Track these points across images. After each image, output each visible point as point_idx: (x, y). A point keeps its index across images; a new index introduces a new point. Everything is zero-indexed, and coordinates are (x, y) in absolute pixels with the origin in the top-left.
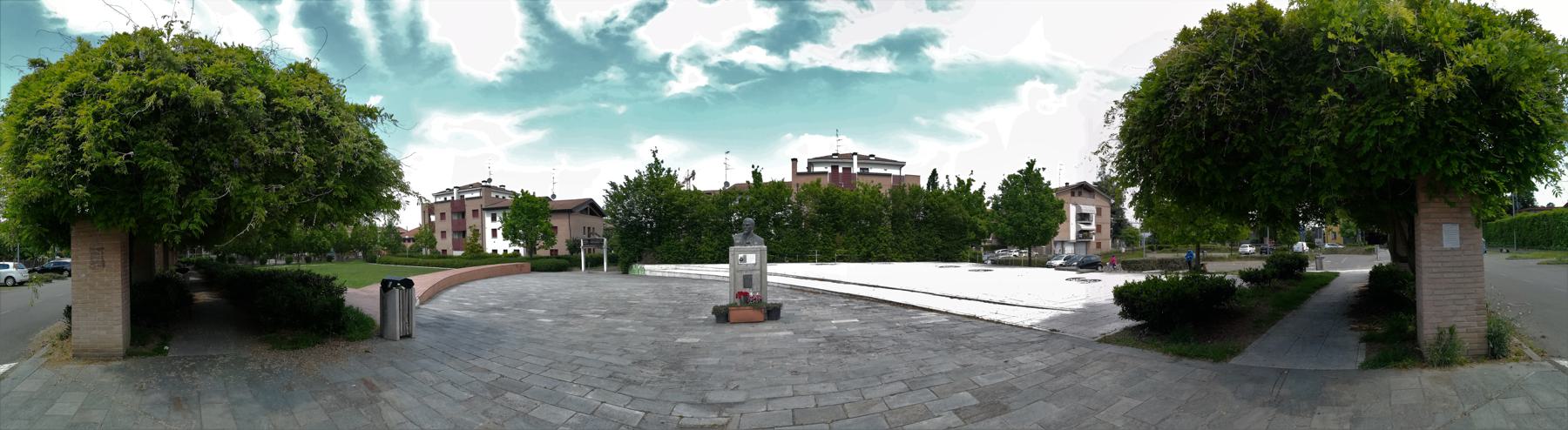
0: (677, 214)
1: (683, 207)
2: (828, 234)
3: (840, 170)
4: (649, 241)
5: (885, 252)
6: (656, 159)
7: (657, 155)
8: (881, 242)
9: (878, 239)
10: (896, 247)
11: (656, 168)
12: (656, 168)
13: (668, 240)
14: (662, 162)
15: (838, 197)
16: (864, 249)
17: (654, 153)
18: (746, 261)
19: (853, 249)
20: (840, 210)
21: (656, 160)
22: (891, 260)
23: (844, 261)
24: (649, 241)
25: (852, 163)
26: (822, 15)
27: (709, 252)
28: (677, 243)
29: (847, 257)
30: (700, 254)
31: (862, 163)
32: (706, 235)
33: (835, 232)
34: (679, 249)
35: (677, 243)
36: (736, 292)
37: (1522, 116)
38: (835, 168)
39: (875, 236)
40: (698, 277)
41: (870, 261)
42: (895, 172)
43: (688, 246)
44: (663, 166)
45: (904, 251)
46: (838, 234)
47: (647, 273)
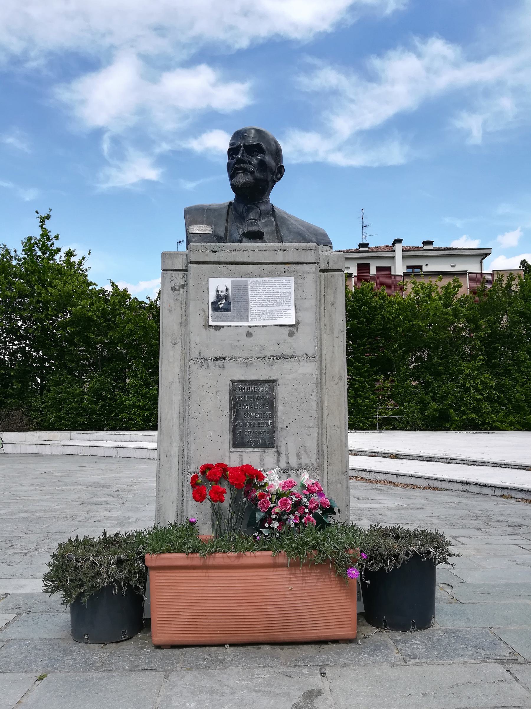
0: (78, 333)
1: (90, 319)
2: (361, 375)
3: (373, 271)
4: (18, 386)
5: (477, 410)
6: (44, 230)
7: (48, 225)
8: (467, 390)
9: (462, 386)
10: (498, 401)
11: (44, 248)
12: (44, 248)
13: (57, 384)
14: (57, 238)
15: (382, 308)
16: (433, 405)
17: (43, 220)
18: (244, 314)
19: (413, 406)
20: (385, 334)
21: (45, 234)
22: (493, 428)
23: (395, 429)
24: (18, 386)
25: (393, 257)
26: (317, 94)
27: (143, 408)
28: (76, 389)
29: (399, 421)
30: (122, 411)
31: (389, 276)
32: (135, 376)
33: (377, 373)
34: (82, 401)
35: (76, 389)
36: (195, 467)
37: (460, 422)
38: (363, 268)
39: (455, 380)
40: (113, 453)
41: (447, 429)
42: (472, 267)
43: (97, 395)
44: (57, 244)
45: (518, 409)
46: (381, 377)
47: (8, 449)
